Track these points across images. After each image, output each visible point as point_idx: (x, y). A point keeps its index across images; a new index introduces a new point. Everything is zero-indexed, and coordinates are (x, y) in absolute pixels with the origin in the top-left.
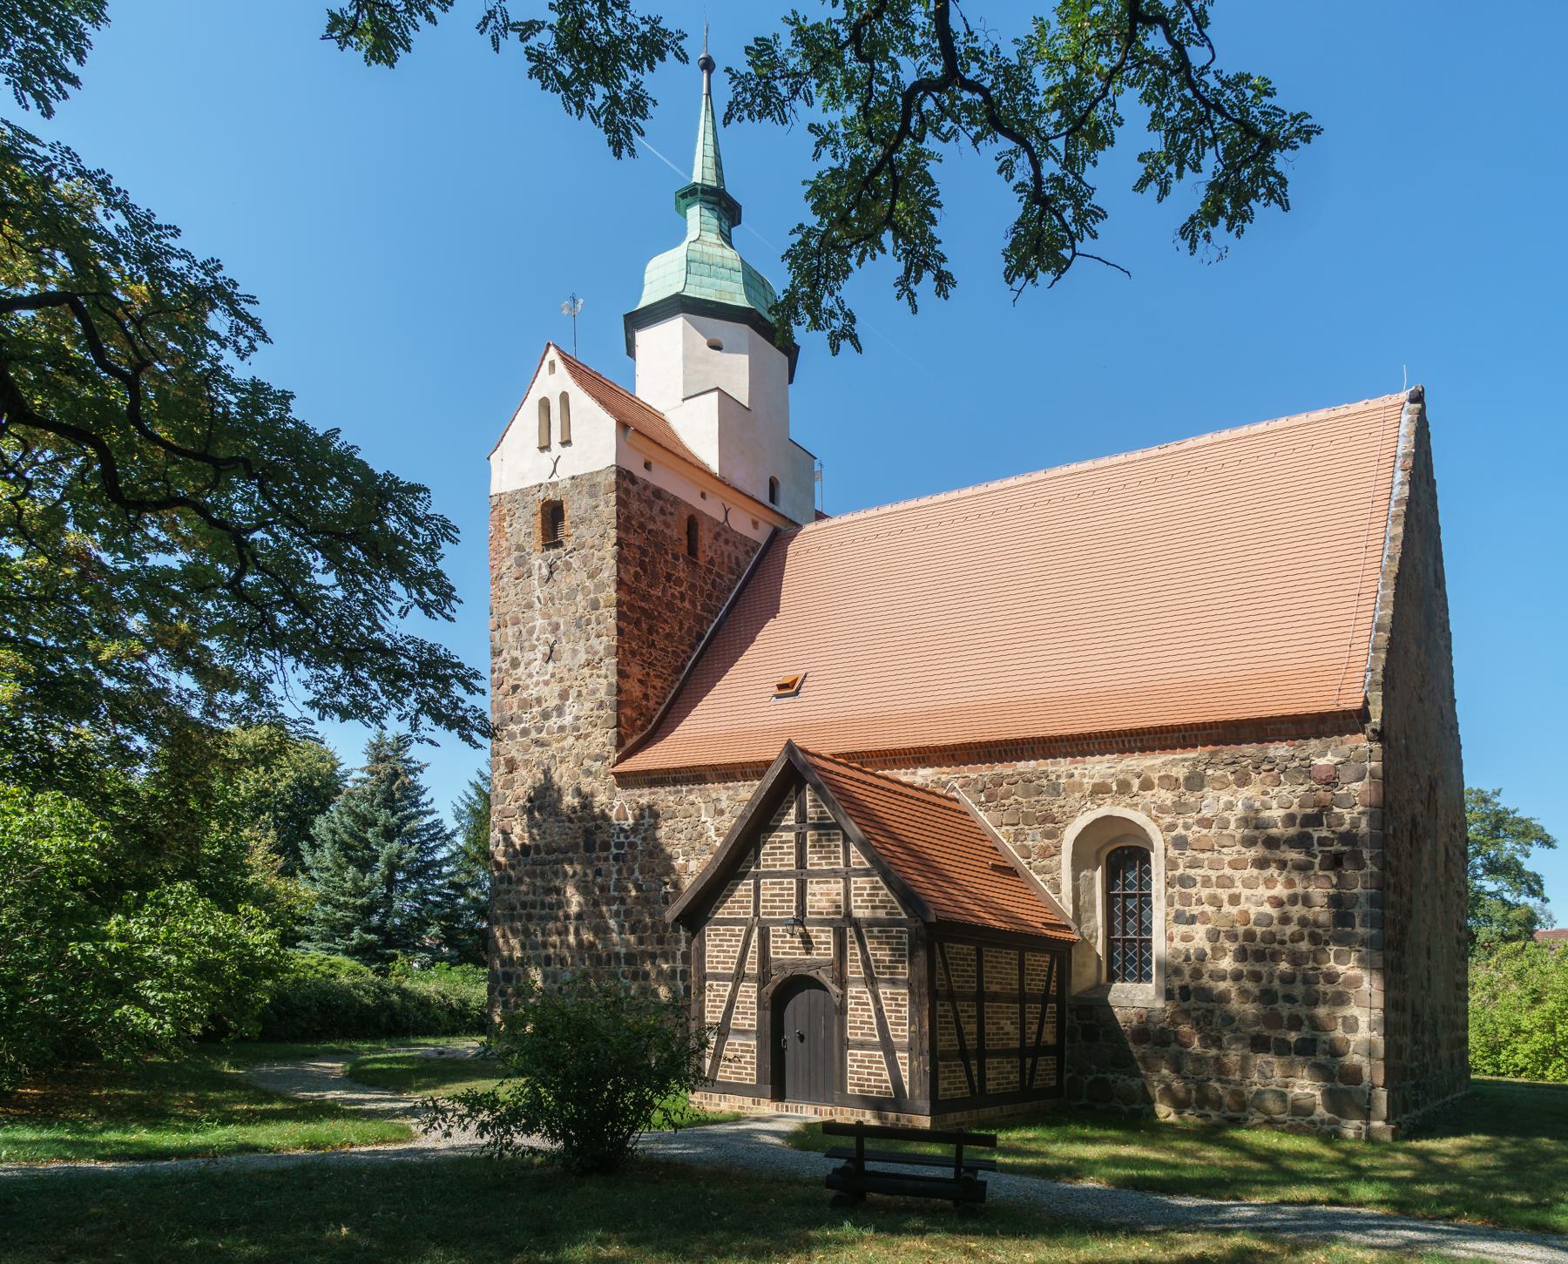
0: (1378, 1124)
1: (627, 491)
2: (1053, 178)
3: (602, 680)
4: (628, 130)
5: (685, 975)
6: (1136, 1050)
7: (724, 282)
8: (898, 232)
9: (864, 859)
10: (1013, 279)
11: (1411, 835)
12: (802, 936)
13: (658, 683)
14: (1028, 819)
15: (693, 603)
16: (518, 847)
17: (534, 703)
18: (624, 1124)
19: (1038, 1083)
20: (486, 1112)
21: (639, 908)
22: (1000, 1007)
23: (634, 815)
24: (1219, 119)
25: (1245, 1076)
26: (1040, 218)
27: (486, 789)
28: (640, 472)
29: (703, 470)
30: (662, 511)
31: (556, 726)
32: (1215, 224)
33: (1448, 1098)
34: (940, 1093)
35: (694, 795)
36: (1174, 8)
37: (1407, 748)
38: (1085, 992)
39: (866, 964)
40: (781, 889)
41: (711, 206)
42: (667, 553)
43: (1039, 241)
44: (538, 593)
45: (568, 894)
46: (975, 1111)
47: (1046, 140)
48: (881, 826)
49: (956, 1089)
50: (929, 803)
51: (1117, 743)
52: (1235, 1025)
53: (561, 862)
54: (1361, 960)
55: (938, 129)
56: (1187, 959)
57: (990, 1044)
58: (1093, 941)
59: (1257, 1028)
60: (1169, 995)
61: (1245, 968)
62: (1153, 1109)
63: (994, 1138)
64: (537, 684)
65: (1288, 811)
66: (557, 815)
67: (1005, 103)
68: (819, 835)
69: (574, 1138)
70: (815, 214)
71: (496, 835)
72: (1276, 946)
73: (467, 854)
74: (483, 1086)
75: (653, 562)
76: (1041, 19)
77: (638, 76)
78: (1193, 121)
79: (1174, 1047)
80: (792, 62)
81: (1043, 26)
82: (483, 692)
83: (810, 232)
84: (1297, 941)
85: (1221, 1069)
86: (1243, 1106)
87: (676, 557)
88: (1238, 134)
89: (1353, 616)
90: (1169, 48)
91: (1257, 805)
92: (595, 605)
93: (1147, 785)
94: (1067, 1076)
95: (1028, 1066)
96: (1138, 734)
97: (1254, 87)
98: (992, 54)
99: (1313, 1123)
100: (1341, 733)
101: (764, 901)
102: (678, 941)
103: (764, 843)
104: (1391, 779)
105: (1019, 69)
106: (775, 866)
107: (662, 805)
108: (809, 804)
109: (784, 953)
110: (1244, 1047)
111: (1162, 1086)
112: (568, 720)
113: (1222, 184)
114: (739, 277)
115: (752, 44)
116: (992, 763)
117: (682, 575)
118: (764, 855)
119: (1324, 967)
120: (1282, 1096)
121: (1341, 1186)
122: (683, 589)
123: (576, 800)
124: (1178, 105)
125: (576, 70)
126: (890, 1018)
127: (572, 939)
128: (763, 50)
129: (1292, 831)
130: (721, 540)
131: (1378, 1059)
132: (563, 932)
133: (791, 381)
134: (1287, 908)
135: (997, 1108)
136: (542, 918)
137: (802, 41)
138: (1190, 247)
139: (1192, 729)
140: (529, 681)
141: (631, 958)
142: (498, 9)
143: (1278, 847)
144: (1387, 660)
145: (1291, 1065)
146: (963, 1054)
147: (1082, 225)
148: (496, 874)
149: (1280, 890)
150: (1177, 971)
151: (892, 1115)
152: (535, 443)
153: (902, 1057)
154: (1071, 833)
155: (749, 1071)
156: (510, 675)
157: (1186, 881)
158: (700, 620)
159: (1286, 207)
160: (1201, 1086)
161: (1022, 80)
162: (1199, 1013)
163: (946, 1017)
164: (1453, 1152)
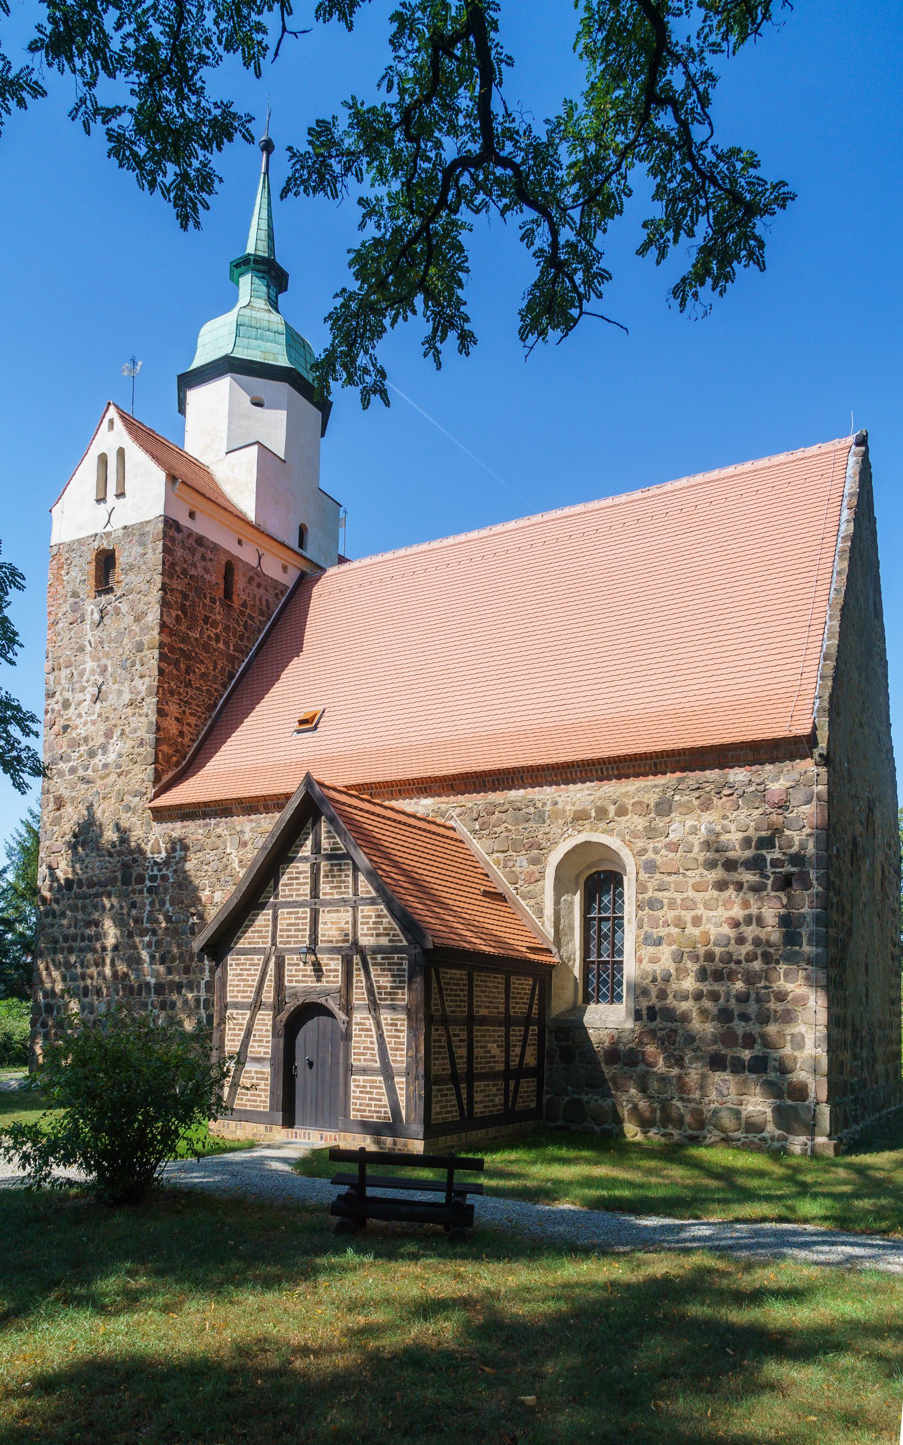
0: (821, 1140)
1: (173, 539)
2: (569, 244)
3: (143, 719)
4: (195, 204)
5: (208, 1003)
6: (608, 1071)
7: (268, 344)
8: (430, 295)
9: (371, 889)
10: (527, 337)
11: (852, 856)
12: (313, 964)
13: (192, 721)
14: (516, 846)
15: (226, 644)
16: (62, 882)
17: (81, 742)
18: (151, 1153)
19: (520, 1105)
20: (29, 1144)
21: (169, 939)
22: (488, 1031)
23: (166, 849)
24: (712, 189)
25: (703, 1096)
26: (554, 281)
27: (35, 826)
28: (185, 521)
29: (241, 518)
30: (203, 558)
31: (101, 764)
32: (702, 284)
33: (884, 1112)
34: (433, 1117)
35: (221, 826)
36: (683, 91)
37: (849, 771)
38: (563, 1014)
39: (370, 991)
40: (296, 918)
41: (261, 275)
42: (205, 597)
43: (551, 301)
44: (89, 637)
45: (106, 927)
46: (463, 1135)
47: (565, 210)
48: (387, 856)
49: (447, 1112)
50: (429, 832)
51: (597, 771)
52: (696, 1044)
53: (98, 895)
54: (807, 978)
55: (472, 202)
56: (654, 980)
57: (478, 1068)
58: (571, 963)
59: (715, 1047)
60: (638, 1015)
61: (706, 987)
62: (622, 1129)
63: (481, 1162)
64: (85, 724)
65: (745, 834)
66: (98, 849)
67: (532, 177)
68: (332, 865)
69: (107, 1169)
70: (357, 279)
71: (43, 871)
72: (733, 966)
73: (16, 890)
74: (28, 1117)
75: (193, 606)
76: (571, 102)
77: (208, 155)
78: (691, 191)
79: (642, 1067)
80: (348, 142)
81: (571, 108)
82: (37, 735)
83: (352, 296)
84: (752, 961)
85: (682, 1087)
86: (701, 1124)
87: (213, 601)
88: (727, 202)
89: (804, 647)
90: (676, 126)
91: (718, 828)
92: (140, 648)
93: (622, 811)
94: (546, 1097)
95: (512, 1088)
96: (615, 762)
97: (742, 160)
98: (525, 134)
99: (763, 1139)
100: (792, 759)
101: (281, 930)
102: (202, 971)
103: (283, 874)
104: (835, 801)
105: (547, 146)
106: (291, 896)
107: (194, 837)
108: (323, 835)
109: (297, 981)
110: (704, 1066)
111: (630, 1106)
112: (111, 757)
113: (711, 247)
114: (282, 339)
115: (314, 126)
116: (486, 792)
117: (218, 617)
118: (283, 885)
119: (775, 987)
120: (737, 1113)
121: (789, 1202)
122: (218, 631)
123: (116, 835)
124: (679, 177)
125: (151, 149)
126: (390, 1043)
127: (108, 971)
128: (323, 131)
129: (749, 853)
130: (254, 584)
131: (822, 1075)
132: (100, 963)
133: (323, 435)
134: (743, 928)
135: (484, 1131)
136: (82, 950)
137: (358, 122)
138: (681, 305)
139: (663, 757)
140: (78, 721)
141: (160, 988)
142: (88, 96)
143: (735, 870)
144: (833, 688)
145: (745, 1082)
146: (454, 1078)
147: (590, 286)
148: (42, 908)
149: (737, 912)
150: (645, 992)
151: (389, 1140)
152: (93, 495)
153: (400, 1082)
154: (554, 858)
155: (263, 1099)
156: (62, 716)
157: (654, 904)
158: (232, 660)
159: (762, 268)
160: (665, 1107)
161: (549, 156)
162: (664, 1033)
163: (440, 1041)
164: (888, 1166)
